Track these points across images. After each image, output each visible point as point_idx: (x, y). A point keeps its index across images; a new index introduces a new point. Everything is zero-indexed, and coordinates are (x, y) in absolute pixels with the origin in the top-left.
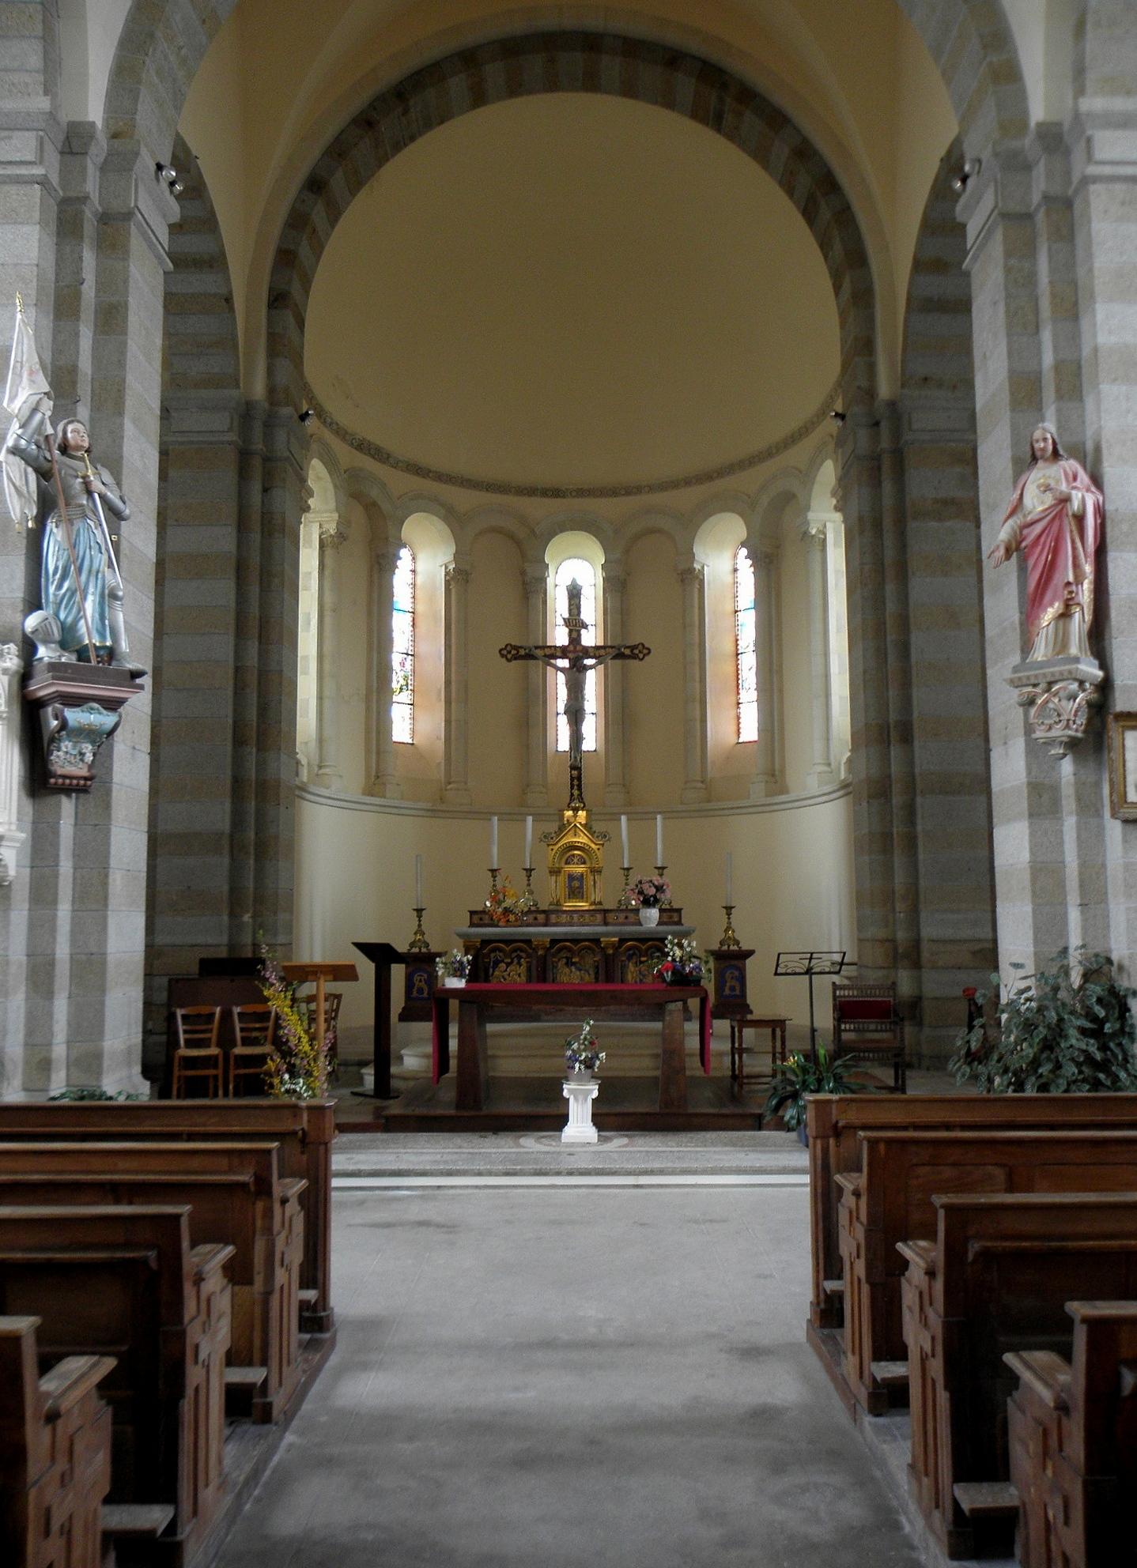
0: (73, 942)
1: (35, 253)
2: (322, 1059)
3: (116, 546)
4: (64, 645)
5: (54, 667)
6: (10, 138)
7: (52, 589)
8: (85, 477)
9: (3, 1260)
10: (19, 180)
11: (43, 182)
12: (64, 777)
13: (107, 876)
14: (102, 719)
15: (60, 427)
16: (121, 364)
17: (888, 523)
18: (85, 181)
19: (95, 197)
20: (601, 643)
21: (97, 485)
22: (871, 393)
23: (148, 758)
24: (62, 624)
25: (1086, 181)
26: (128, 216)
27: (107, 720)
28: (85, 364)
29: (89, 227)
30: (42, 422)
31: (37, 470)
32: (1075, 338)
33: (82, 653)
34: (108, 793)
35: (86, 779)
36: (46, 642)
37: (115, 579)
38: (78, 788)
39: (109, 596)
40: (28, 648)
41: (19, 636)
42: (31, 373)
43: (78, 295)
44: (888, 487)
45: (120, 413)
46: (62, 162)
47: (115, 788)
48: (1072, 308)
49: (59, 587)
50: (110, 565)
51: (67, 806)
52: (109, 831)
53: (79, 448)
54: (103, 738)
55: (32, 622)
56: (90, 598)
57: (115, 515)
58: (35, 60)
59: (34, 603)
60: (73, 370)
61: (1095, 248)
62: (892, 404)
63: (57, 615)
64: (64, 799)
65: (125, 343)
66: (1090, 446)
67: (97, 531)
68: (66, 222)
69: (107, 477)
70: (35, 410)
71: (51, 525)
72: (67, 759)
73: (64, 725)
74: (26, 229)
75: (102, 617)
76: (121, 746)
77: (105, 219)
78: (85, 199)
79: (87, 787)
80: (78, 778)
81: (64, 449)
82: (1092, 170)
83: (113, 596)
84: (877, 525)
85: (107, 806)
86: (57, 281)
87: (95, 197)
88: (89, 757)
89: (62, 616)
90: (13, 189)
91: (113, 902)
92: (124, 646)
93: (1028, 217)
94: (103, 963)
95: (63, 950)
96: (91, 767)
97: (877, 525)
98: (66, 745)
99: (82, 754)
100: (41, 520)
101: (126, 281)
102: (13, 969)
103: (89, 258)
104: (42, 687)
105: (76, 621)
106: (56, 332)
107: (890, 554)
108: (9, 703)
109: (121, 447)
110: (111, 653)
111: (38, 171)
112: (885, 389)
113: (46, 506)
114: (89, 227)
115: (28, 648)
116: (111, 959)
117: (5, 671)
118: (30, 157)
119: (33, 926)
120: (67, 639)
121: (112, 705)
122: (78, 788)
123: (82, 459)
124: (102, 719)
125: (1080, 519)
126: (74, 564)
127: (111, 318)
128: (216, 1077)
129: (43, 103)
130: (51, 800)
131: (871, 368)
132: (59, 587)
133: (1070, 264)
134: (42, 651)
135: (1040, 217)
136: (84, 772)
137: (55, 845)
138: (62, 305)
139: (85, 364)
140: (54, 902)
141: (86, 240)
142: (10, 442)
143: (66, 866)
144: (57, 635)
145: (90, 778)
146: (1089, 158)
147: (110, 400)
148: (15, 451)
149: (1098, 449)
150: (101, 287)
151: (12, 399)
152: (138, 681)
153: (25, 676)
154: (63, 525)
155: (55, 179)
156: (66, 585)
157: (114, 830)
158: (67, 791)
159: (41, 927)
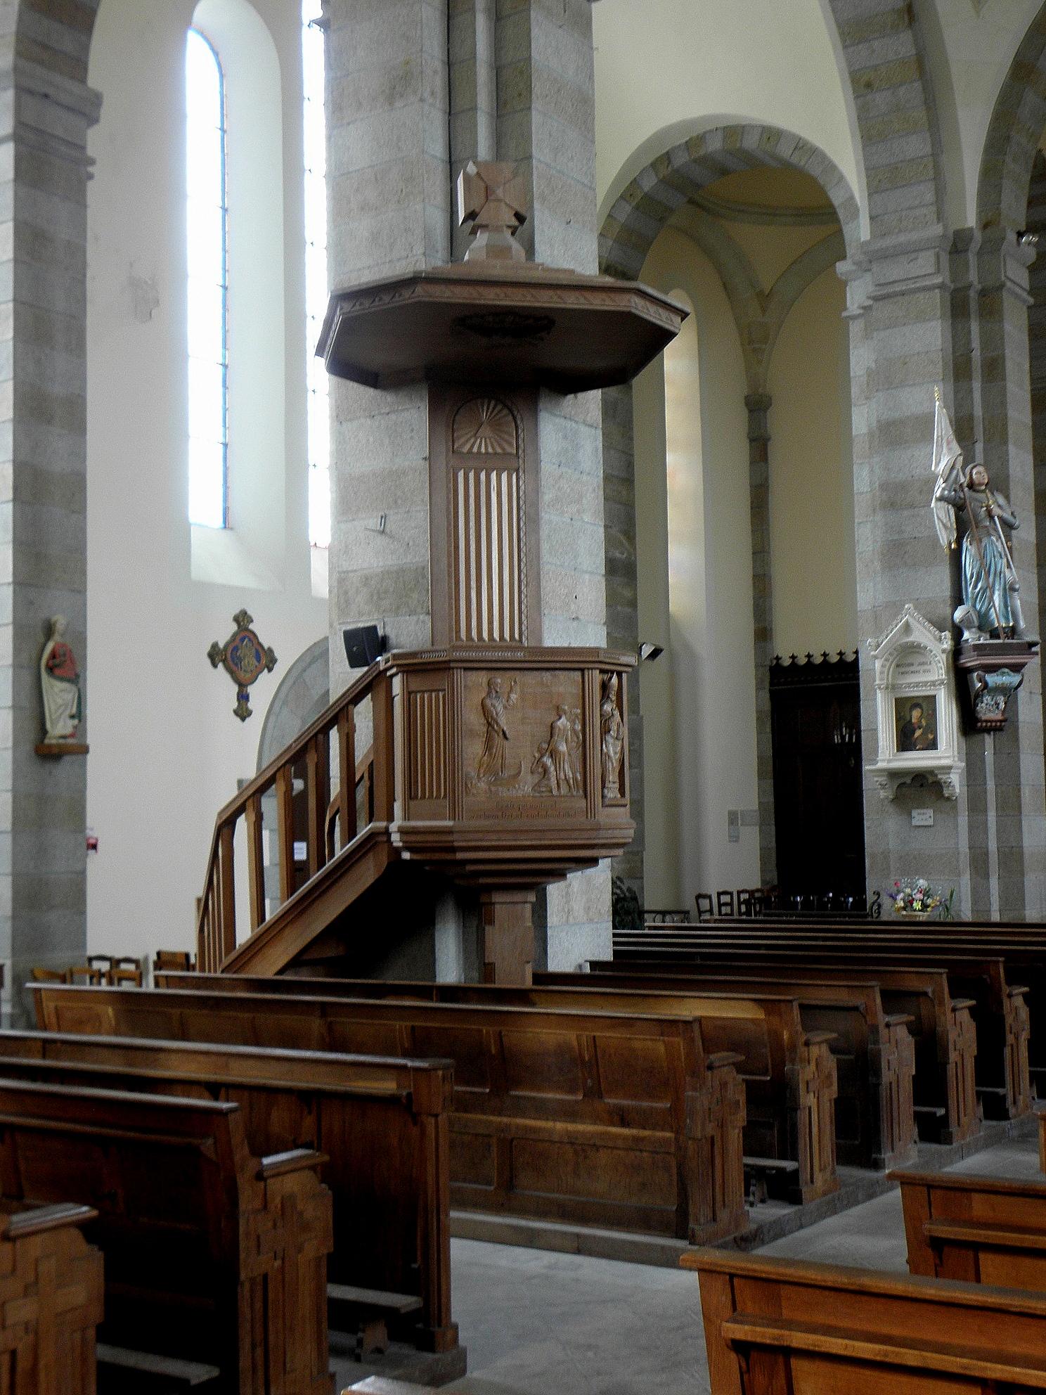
0: (998, 839)
1: (939, 342)
2: (749, 1304)
3: (1010, 549)
4: (980, 628)
5: (977, 648)
6: (916, 259)
7: (970, 589)
8: (988, 506)
10: (925, 289)
11: (941, 287)
12: (986, 721)
13: (1019, 790)
14: (1010, 679)
15: (968, 470)
16: (1003, 404)
18: (968, 271)
19: (976, 283)
21: (996, 511)
23: (1040, 697)
24: (979, 612)
26: (1002, 286)
27: (1014, 679)
28: (978, 411)
29: (973, 305)
30: (957, 475)
31: (954, 506)
33: (994, 634)
34: (1017, 729)
35: (1001, 721)
36: (969, 628)
37: (1010, 575)
38: (995, 728)
39: (1010, 589)
40: (957, 632)
41: (949, 624)
42: (948, 443)
43: (969, 361)
45: (1005, 443)
46: (951, 260)
47: (1021, 725)
49: (975, 587)
50: (1009, 566)
51: (989, 740)
52: (1018, 758)
53: (980, 484)
54: (1010, 693)
55: (959, 614)
56: (997, 593)
57: (1008, 526)
58: (930, 197)
59: (958, 600)
60: (971, 418)
61: (858, 1266)
63: (974, 606)
64: (986, 736)
65: (1004, 388)
67: (997, 543)
68: (958, 308)
69: (1001, 500)
70: (953, 468)
71: (966, 543)
72: (988, 709)
73: (986, 685)
74: (934, 323)
75: (1006, 606)
76: (1022, 694)
77: (983, 293)
78: (970, 286)
79: (1004, 727)
80: (996, 721)
81: (971, 486)
83: (1013, 589)
85: (1017, 739)
86: (954, 352)
87: (976, 283)
88: (1002, 706)
89: (978, 607)
90: (921, 296)
91: (1025, 810)
92: (1022, 625)
94: (1021, 854)
95: (993, 845)
96: (1004, 712)
98: (987, 699)
99: (997, 704)
100: (959, 541)
101: (1002, 338)
102: (962, 857)
103: (975, 327)
104: (969, 661)
105: (988, 610)
106: (956, 392)
108: (947, 673)
109: (1007, 468)
110: (1013, 631)
111: (938, 280)
113: (962, 527)
114: (973, 305)
115: (957, 632)
116: (1025, 850)
117: (944, 651)
118: (932, 270)
119: (971, 827)
120: (983, 624)
121: (1017, 668)
122: (995, 728)
123: (983, 491)
124: (1010, 679)
126: (984, 569)
127: (994, 369)
128: (732, 914)
129: (938, 230)
130: (978, 737)
132: (975, 587)
134: (966, 635)
136: (1000, 717)
137: (983, 770)
138: (959, 370)
139: (978, 411)
140: (985, 811)
141: (972, 316)
142: (938, 494)
143: (991, 785)
144: (976, 623)
145: (1005, 720)
147: (997, 432)
148: (941, 499)
150: (985, 345)
151: (937, 465)
152: (1034, 649)
153: (957, 652)
154: (975, 543)
155: (948, 282)
156: (979, 586)
157: (1022, 757)
158: (988, 730)
159: (978, 828)
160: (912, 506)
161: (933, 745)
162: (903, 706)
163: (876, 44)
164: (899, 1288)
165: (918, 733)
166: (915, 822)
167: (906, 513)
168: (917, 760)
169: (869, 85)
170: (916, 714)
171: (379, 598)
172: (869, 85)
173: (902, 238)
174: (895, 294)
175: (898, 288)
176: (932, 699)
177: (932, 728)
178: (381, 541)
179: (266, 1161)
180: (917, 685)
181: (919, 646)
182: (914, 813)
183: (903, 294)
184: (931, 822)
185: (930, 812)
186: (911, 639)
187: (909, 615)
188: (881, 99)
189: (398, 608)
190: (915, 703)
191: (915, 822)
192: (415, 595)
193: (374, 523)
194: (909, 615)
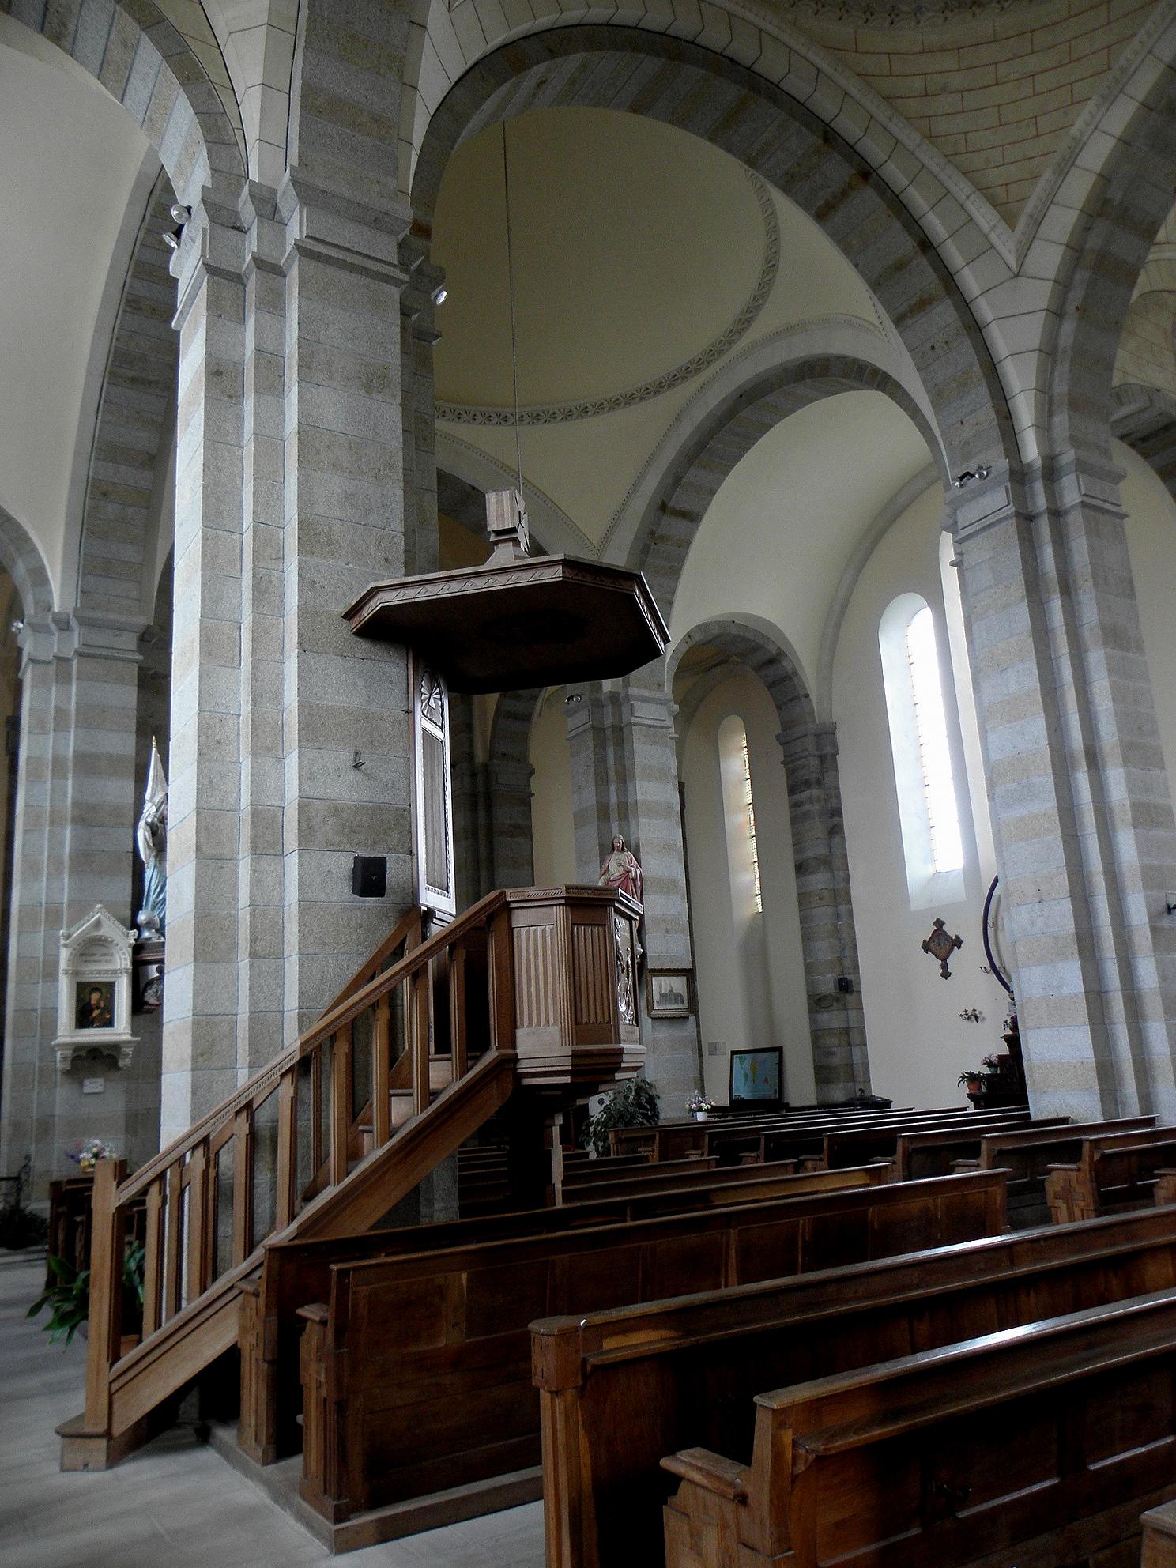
9: (1172, 1233)
17: (482, 835)
20: (524, 1067)
22: (471, 756)
25: (630, 724)
32: (625, 791)
36: (150, 929)
44: (482, 813)
48: (624, 777)
62: (485, 766)
66: (633, 843)
82: (634, 720)
84: (475, 834)
90: (121, 664)
93: (238, 279)
97: (475, 834)
107: (483, 854)
112: (480, 756)
125: (635, 880)
131: (471, 741)
133: (623, 757)
135: (252, 283)
146: (632, 715)
149: (638, 846)
156: (79, 1283)
160: (102, 825)
161: (109, 1023)
162: (83, 991)
163: (123, 468)
164: (552, 1503)
165: (96, 1013)
166: (86, 1090)
167: (96, 829)
168: (94, 1035)
169: (105, 494)
170: (95, 996)
171: (351, 831)
172: (105, 494)
173: (112, 616)
174: (100, 656)
175: (104, 652)
176: (111, 986)
177: (109, 1008)
178: (353, 775)
179: (1054, 1481)
180: (99, 972)
181: (106, 940)
182: (87, 1082)
183: (106, 658)
184: (100, 1089)
185: (100, 1081)
186: (100, 933)
187: (98, 913)
188: (111, 509)
189: (374, 843)
190: (96, 987)
191: (86, 1090)
192: (395, 835)
193: (345, 757)
194: (98, 913)
